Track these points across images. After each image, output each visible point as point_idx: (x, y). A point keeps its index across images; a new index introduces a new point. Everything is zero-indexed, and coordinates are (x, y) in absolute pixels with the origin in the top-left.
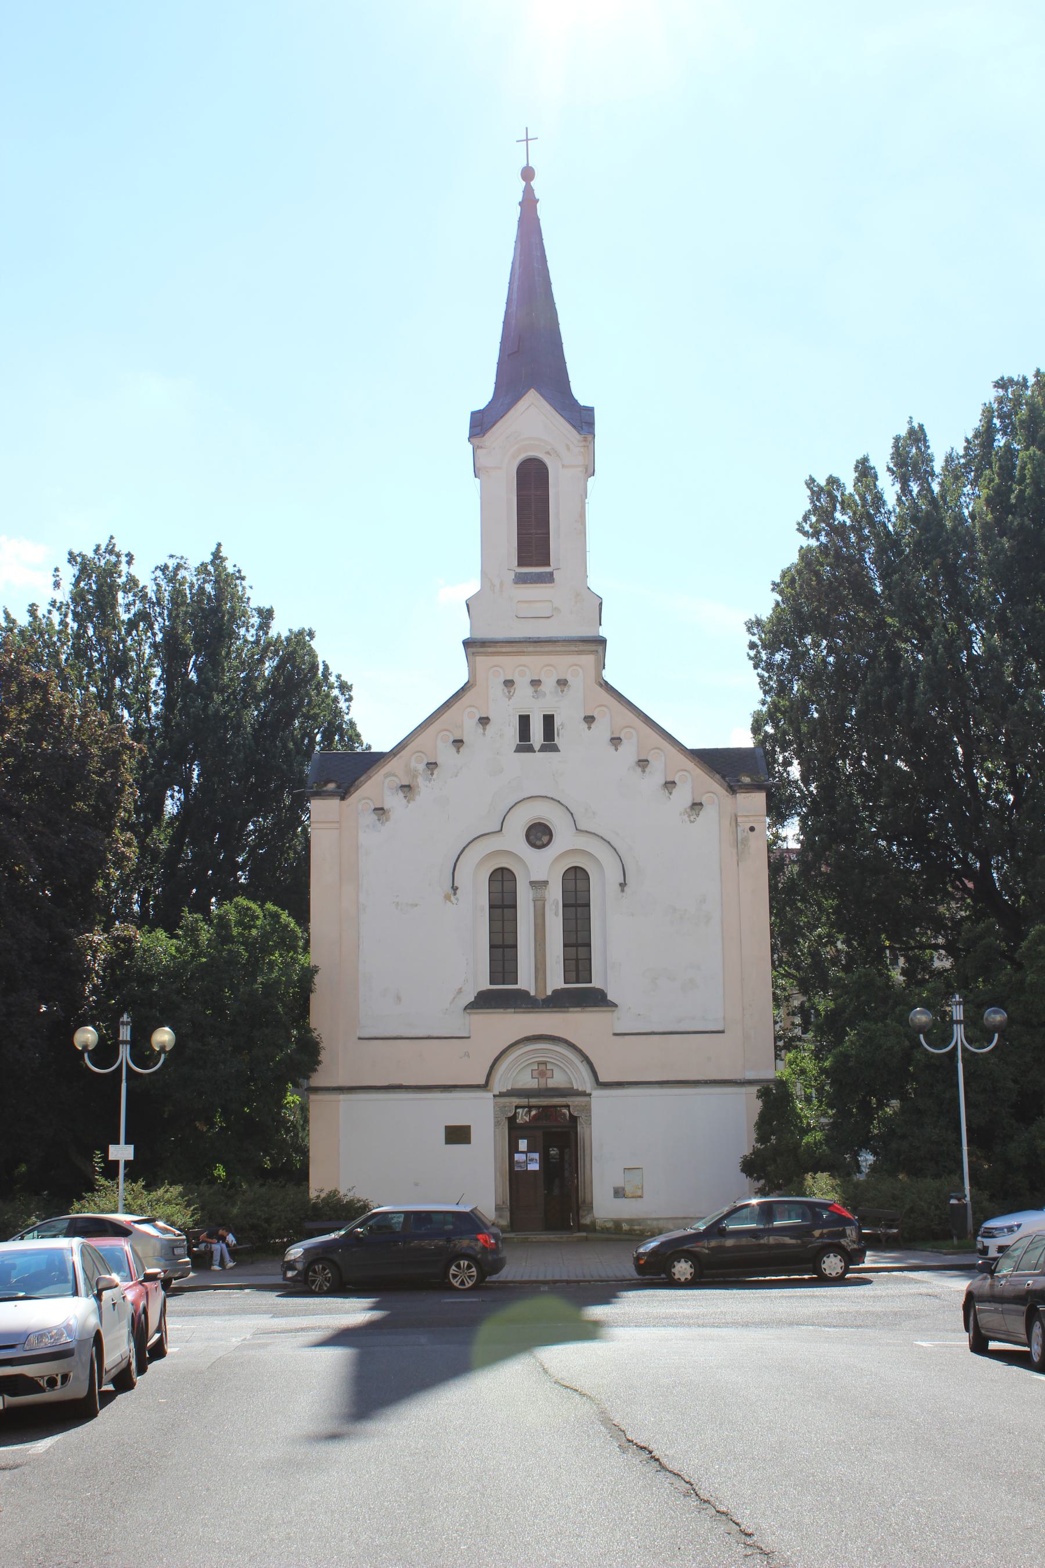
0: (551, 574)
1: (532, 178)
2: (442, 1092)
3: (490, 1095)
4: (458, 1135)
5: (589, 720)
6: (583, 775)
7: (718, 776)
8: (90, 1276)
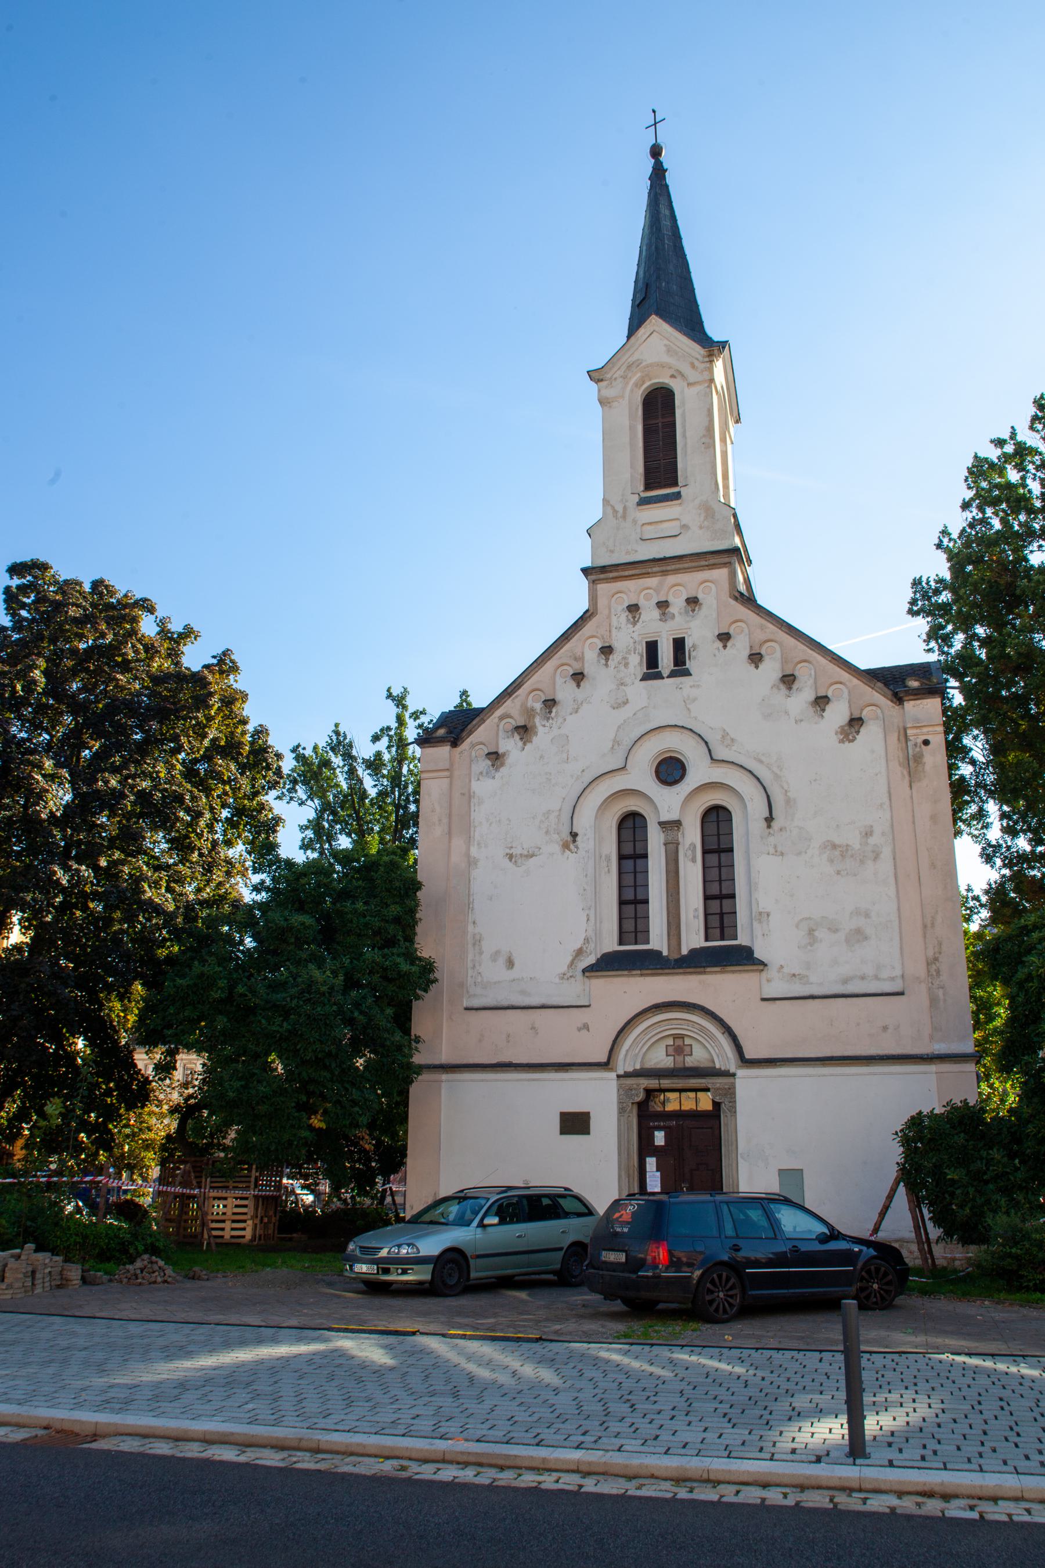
0: (679, 493)
1: (660, 154)
2: (556, 1071)
3: (613, 1075)
4: (575, 1123)
5: (724, 638)
6: (725, 702)
7: (879, 684)
8: (427, 1218)
